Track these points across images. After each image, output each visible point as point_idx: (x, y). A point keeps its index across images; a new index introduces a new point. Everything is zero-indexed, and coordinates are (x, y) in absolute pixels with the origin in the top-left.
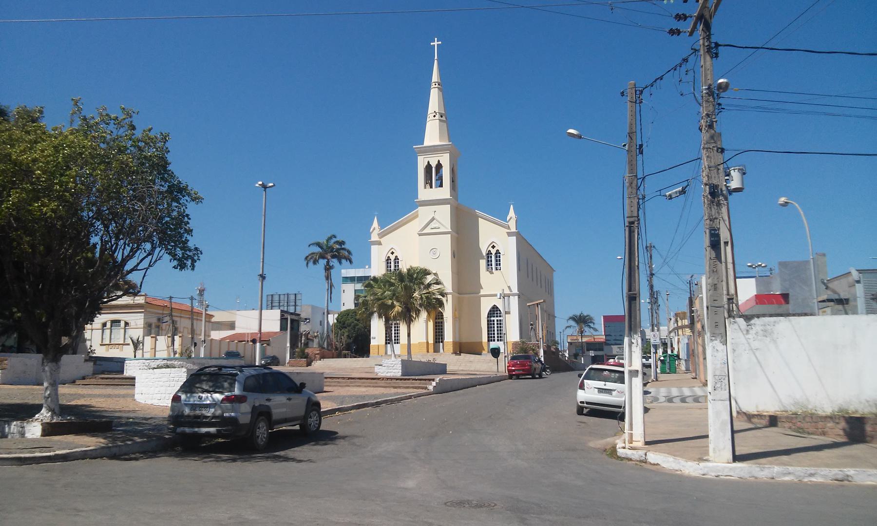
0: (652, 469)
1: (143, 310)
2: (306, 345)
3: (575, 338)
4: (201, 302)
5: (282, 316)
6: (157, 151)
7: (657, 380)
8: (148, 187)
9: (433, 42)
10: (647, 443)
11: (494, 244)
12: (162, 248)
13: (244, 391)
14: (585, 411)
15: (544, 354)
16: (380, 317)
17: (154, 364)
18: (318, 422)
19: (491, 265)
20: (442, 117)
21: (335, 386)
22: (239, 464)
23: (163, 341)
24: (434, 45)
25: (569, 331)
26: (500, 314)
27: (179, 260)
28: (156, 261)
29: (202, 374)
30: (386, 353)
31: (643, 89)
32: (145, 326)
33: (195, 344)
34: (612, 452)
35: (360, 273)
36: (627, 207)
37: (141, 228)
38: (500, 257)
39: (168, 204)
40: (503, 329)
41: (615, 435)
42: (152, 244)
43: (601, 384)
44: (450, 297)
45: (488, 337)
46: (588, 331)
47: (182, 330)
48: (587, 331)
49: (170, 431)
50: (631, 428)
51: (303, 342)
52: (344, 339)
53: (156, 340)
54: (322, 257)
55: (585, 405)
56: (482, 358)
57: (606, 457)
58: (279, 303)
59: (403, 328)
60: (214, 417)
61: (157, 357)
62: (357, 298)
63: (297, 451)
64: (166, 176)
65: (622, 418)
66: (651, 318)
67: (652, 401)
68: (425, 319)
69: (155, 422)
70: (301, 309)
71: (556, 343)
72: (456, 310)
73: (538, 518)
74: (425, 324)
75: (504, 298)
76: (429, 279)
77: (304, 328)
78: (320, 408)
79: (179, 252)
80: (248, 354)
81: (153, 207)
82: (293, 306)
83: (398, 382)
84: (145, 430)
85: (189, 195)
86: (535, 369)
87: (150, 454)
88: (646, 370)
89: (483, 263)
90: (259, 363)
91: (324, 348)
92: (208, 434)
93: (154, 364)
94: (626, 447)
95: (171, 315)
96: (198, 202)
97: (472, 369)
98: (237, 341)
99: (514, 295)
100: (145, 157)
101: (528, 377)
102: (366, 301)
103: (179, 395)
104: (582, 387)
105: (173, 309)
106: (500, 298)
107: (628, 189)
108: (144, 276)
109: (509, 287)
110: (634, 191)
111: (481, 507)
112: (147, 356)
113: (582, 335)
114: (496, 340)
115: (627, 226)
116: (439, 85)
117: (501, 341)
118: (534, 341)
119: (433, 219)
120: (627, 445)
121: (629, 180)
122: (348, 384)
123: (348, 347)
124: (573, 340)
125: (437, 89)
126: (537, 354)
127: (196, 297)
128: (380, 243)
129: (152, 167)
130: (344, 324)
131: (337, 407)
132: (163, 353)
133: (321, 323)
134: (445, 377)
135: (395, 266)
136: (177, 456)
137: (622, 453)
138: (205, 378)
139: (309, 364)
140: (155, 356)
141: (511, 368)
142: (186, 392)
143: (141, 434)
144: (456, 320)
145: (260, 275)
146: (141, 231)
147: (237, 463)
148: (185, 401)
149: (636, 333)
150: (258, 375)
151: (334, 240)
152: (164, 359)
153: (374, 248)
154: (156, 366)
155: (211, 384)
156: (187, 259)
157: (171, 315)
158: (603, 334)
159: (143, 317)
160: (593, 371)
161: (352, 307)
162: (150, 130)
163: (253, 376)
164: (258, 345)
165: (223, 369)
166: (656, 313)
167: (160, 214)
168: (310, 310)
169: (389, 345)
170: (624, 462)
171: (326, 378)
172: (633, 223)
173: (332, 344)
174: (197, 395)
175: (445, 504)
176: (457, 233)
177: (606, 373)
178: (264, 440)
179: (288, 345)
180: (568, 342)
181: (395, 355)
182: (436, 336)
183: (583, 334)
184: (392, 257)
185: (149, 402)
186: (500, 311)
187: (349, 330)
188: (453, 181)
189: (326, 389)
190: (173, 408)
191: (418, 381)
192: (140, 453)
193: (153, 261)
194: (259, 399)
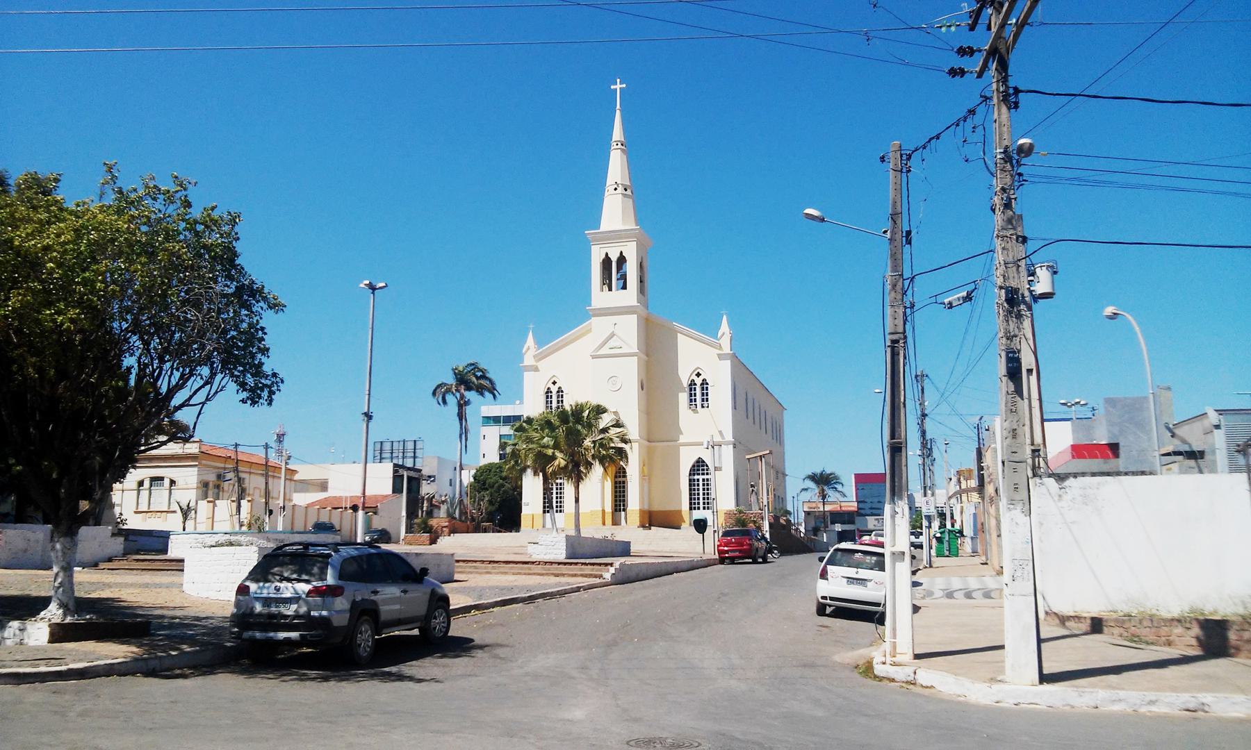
2: (430, 514)
3: (814, 505)
4: (279, 452)
5: (395, 472)
7: (931, 566)
8: (207, 288)
12: (226, 374)
13: (340, 579)
14: (828, 610)
15: (770, 528)
16: (536, 473)
18: (445, 625)
19: (695, 400)
20: (626, 190)
21: (471, 573)
22: (332, 683)
23: (224, 507)
24: (616, 89)
25: (806, 496)
26: (707, 470)
27: (252, 390)
28: (216, 392)
33: (271, 512)
34: (867, 669)
37: (195, 346)
39: (235, 311)
41: (871, 645)
42: (212, 368)
43: (851, 572)
45: (691, 504)
46: (832, 495)
47: (251, 493)
51: (425, 509)
53: (215, 505)
55: (828, 601)
57: (858, 676)
58: (392, 453)
59: (569, 489)
60: (297, 616)
62: (503, 446)
64: (233, 272)
68: (600, 478)
72: (644, 465)
74: (599, 484)
75: (713, 447)
76: (606, 420)
77: (426, 489)
78: (448, 605)
79: (250, 380)
81: (213, 317)
84: (197, 635)
85: (265, 299)
86: (757, 549)
87: (205, 669)
88: (916, 552)
89: (683, 398)
91: (455, 518)
92: (287, 640)
95: (236, 470)
96: (278, 310)
97: (668, 550)
98: (330, 509)
99: (727, 443)
100: (205, 247)
101: (747, 560)
105: (239, 462)
109: (720, 432)
110: (899, 297)
112: (201, 528)
113: (824, 502)
114: (701, 508)
115: (889, 346)
117: (708, 508)
118: (755, 510)
119: (612, 335)
122: (489, 570)
124: (811, 508)
126: (759, 528)
128: (536, 369)
130: (484, 484)
135: (558, 402)
140: (212, 529)
142: (257, 581)
143: (191, 640)
146: (196, 349)
148: (256, 593)
149: (901, 498)
150: (360, 557)
152: (226, 533)
153: (528, 376)
159: (196, 473)
160: (840, 553)
161: (496, 460)
162: (213, 209)
163: (353, 558)
165: (310, 547)
167: (223, 326)
171: (458, 561)
172: (897, 341)
175: (628, 743)
176: (647, 355)
177: (858, 555)
179: (404, 513)
182: (616, 501)
183: (825, 500)
184: (554, 389)
185: (204, 595)
186: (707, 466)
189: (457, 577)
190: (238, 604)
191: (589, 567)
192: (190, 668)
193: (212, 393)
194: (361, 591)
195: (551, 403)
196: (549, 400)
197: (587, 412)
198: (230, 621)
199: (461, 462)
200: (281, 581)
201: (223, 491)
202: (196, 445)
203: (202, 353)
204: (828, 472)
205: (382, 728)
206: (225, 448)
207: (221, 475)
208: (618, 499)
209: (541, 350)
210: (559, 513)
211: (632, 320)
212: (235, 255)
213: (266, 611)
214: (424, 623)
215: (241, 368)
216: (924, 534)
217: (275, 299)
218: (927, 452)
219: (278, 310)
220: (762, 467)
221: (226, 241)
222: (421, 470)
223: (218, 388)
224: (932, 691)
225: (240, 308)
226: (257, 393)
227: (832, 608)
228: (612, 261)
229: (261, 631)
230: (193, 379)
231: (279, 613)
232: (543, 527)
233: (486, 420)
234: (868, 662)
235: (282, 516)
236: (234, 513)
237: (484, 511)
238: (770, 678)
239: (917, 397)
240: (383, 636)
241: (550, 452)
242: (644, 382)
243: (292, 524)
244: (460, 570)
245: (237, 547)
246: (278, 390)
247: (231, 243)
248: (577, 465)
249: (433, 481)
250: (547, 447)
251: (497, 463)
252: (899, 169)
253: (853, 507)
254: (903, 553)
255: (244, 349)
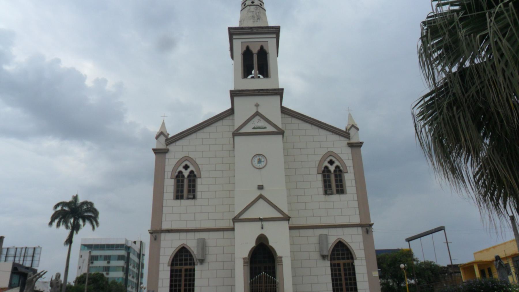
196: (192, 183)
208: (178, 283)
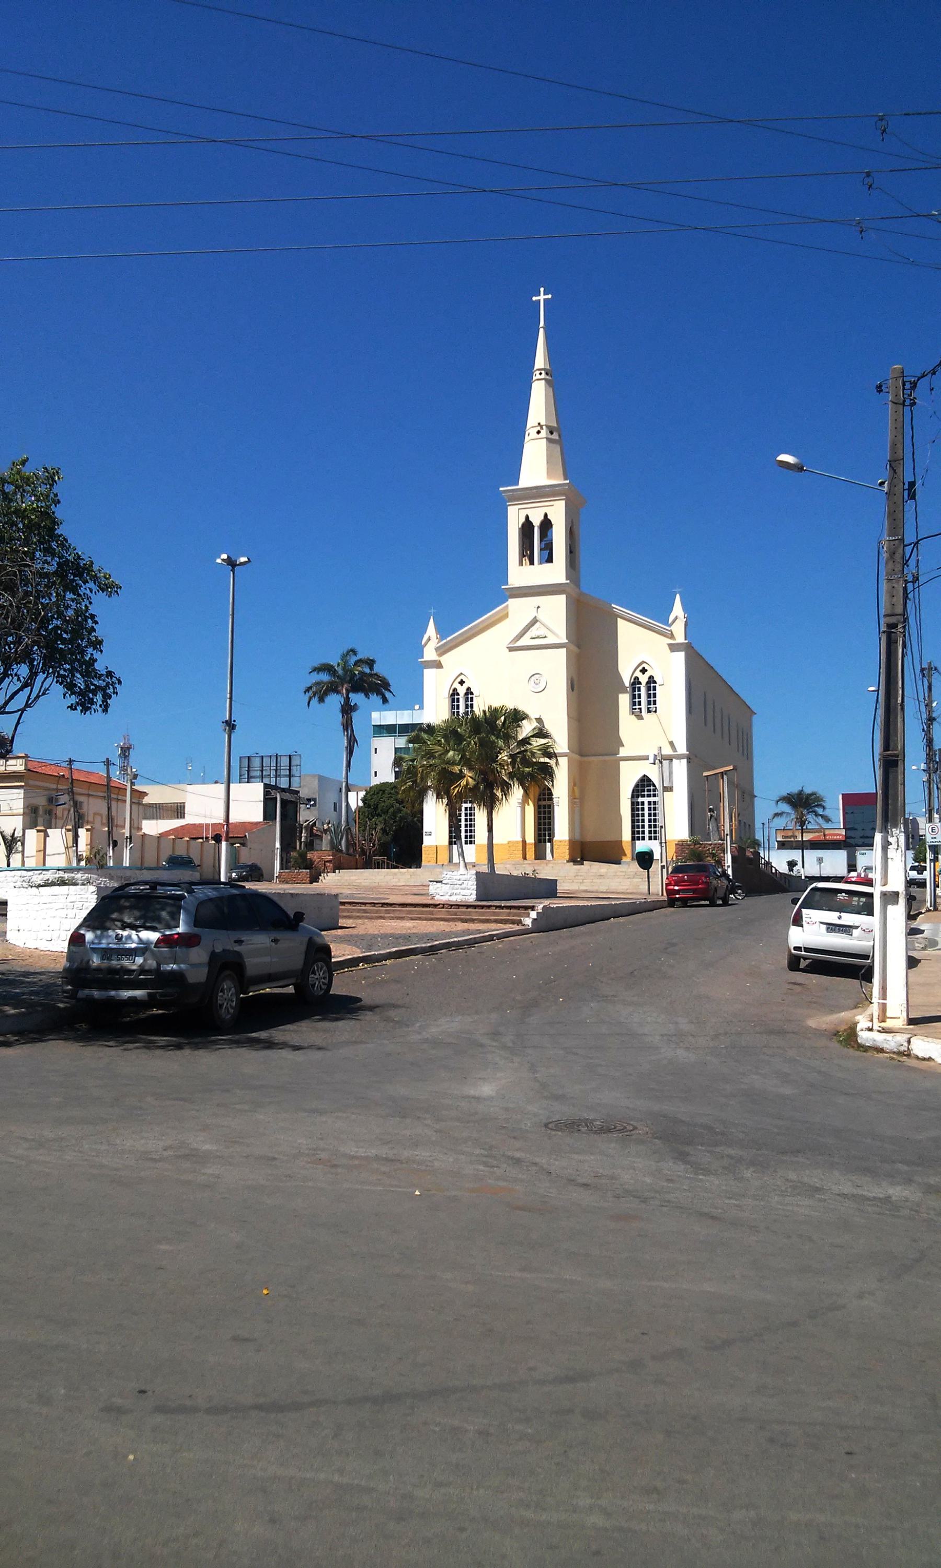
0: (920, 1067)
1: (23, 784)
2: (310, 846)
3: (790, 834)
4: (124, 769)
5: (266, 793)
6: (38, 500)
7: (936, 909)
8: (22, 565)
9: (548, 299)
10: (911, 1021)
11: (644, 665)
12: (48, 673)
13: (195, 926)
14: (803, 964)
15: (733, 862)
16: (439, 796)
17: (38, 878)
18: (326, 981)
19: (640, 703)
20: (551, 433)
21: (359, 918)
22: (187, 1052)
23: (57, 838)
24: (539, 301)
25: (780, 823)
26: (654, 790)
27: (82, 693)
28: (38, 697)
29: (121, 897)
30: (451, 860)
31: (918, 380)
32: (27, 810)
33: (115, 844)
34: (851, 1033)
35: (404, 717)
36: (884, 598)
37: (10, 639)
38: (655, 688)
39: (58, 595)
40: (659, 817)
41: (856, 1007)
42: (31, 667)
43: (832, 917)
44: (563, 761)
45: (633, 833)
46: (812, 822)
47: (91, 819)
48: (811, 820)
49: (65, 995)
50: (884, 995)
51: (303, 839)
52: (376, 834)
53: (46, 835)
54: (332, 688)
55: (803, 953)
56: (621, 870)
57: (837, 1045)
58: (262, 771)
59: (480, 816)
60: (142, 970)
61: (48, 865)
62: (398, 762)
63: (289, 1031)
64: (54, 545)
65: (868, 976)
66: (927, 799)
67: (926, 946)
68: (520, 801)
69: (40, 980)
70: (300, 783)
71: (756, 844)
72: (575, 785)
73: (708, 1152)
74: (519, 809)
75: (661, 762)
76: (526, 729)
77: (305, 815)
78: (330, 957)
79: (80, 682)
80: (208, 861)
81: (30, 603)
82: (285, 776)
83: (470, 912)
84: (24, 994)
85: (95, 579)
86: (716, 888)
87: (32, 1036)
88: (914, 890)
89: (624, 700)
90: (226, 879)
91: (341, 851)
92: (133, 1000)
93: (38, 878)
94: (874, 1028)
95: (72, 793)
96: (111, 592)
97: (603, 888)
98: (188, 839)
99: (679, 757)
100: (17, 512)
101: (703, 902)
102: (414, 767)
103: (82, 932)
104: (798, 921)
105: (75, 782)
106: (655, 764)
107: (886, 563)
108: (18, 723)
109: (671, 743)
110: (898, 567)
111: (609, 1131)
112: (30, 863)
113: (802, 829)
114: (647, 838)
115: (884, 632)
116: (547, 374)
117: (655, 838)
118: (715, 840)
119: (534, 621)
120: (877, 1025)
121: (889, 548)
122: (382, 915)
123: (384, 850)
124: (787, 837)
125: (543, 381)
126: (720, 863)
127: (117, 761)
128: (438, 665)
129: (30, 527)
130: (376, 808)
131: (361, 955)
132: (57, 859)
133: (336, 807)
134: (554, 903)
135: (467, 707)
136: (77, 1039)
137: (867, 1040)
138: (127, 904)
139: (314, 879)
140: (44, 864)
141: (672, 887)
142: (93, 928)
143: (16, 1001)
144: (575, 802)
145: (226, 722)
146: (12, 643)
147: (183, 1051)
148: (93, 943)
149: (896, 826)
150: (220, 899)
151: (353, 659)
152: (59, 870)
153: (428, 674)
154: (41, 883)
155: (137, 913)
156: (94, 693)
157: (72, 792)
158: (842, 827)
159: (22, 796)
160: (818, 893)
161: (391, 779)
162: (24, 463)
163: (211, 900)
164: (224, 844)
165: (158, 887)
166: (938, 788)
167: (43, 613)
168: (316, 782)
169: (455, 847)
170: (869, 1054)
171: (343, 904)
172: (895, 626)
173: (355, 844)
174: (111, 933)
175: (546, 1125)
176: (579, 646)
177: (842, 896)
178: (232, 1011)
179: (278, 845)
180: (777, 841)
181: (466, 865)
182: (539, 830)
183: (805, 827)
184: (462, 690)
185: (31, 945)
186: (654, 785)
187: (385, 820)
188: (572, 551)
189: (342, 922)
190: (70, 956)
191: (505, 911)
192: (14, 1034)
193: (32, 697)
194: (222, 941)
195: (458, 708)
197: (503, 718)
198: (62, 978)
199: (347, 782)
200: (123, 928)
201: (56, 818)
202: (20, 761)
203: (18, 648)
204: (808, 790)
205: (246, 1107)
206: (56, 765)
207: (52, 797)
209: (445, 641)
210: (469, 845)
211: (560, 601)
212: (55, 522)
213: (106, 964)
214: (301, 978)
215: (68, 667)
216: (928, 868)
217: (107, 579)
218: (934, 766)
219: (111, 592)
220: (724, 787)
221: (43, 504)
222: (299, 792)
223: (40, 692)
224: (932, 1063)
225: (64, 592)
226: (89, 697)
227: (808, 961)
228: (533, 527)
229: (100, 988)
230: (7, 680)
231: (122, 967)
232: (450, 862)
233: (377, 728)
234: (850, 1028)
235: (128, 848)
236: (70, 844)
237: (376, 842)
238: (726, 1047)
239: (921, 698)
240: (251, 994)
241: (456, 769)
242: (575, 683)
243: (142, 857)
244: (345, 914)
245: (71, 887)
246: (114, 693)
247: (48, 507)
248: (490, 786)
249: (314, 805)
250: (454, 763)
251: (391, 783)
252: (901, 402)
253: (839, 835)
254: (897, 894)
255: (71, 641)
